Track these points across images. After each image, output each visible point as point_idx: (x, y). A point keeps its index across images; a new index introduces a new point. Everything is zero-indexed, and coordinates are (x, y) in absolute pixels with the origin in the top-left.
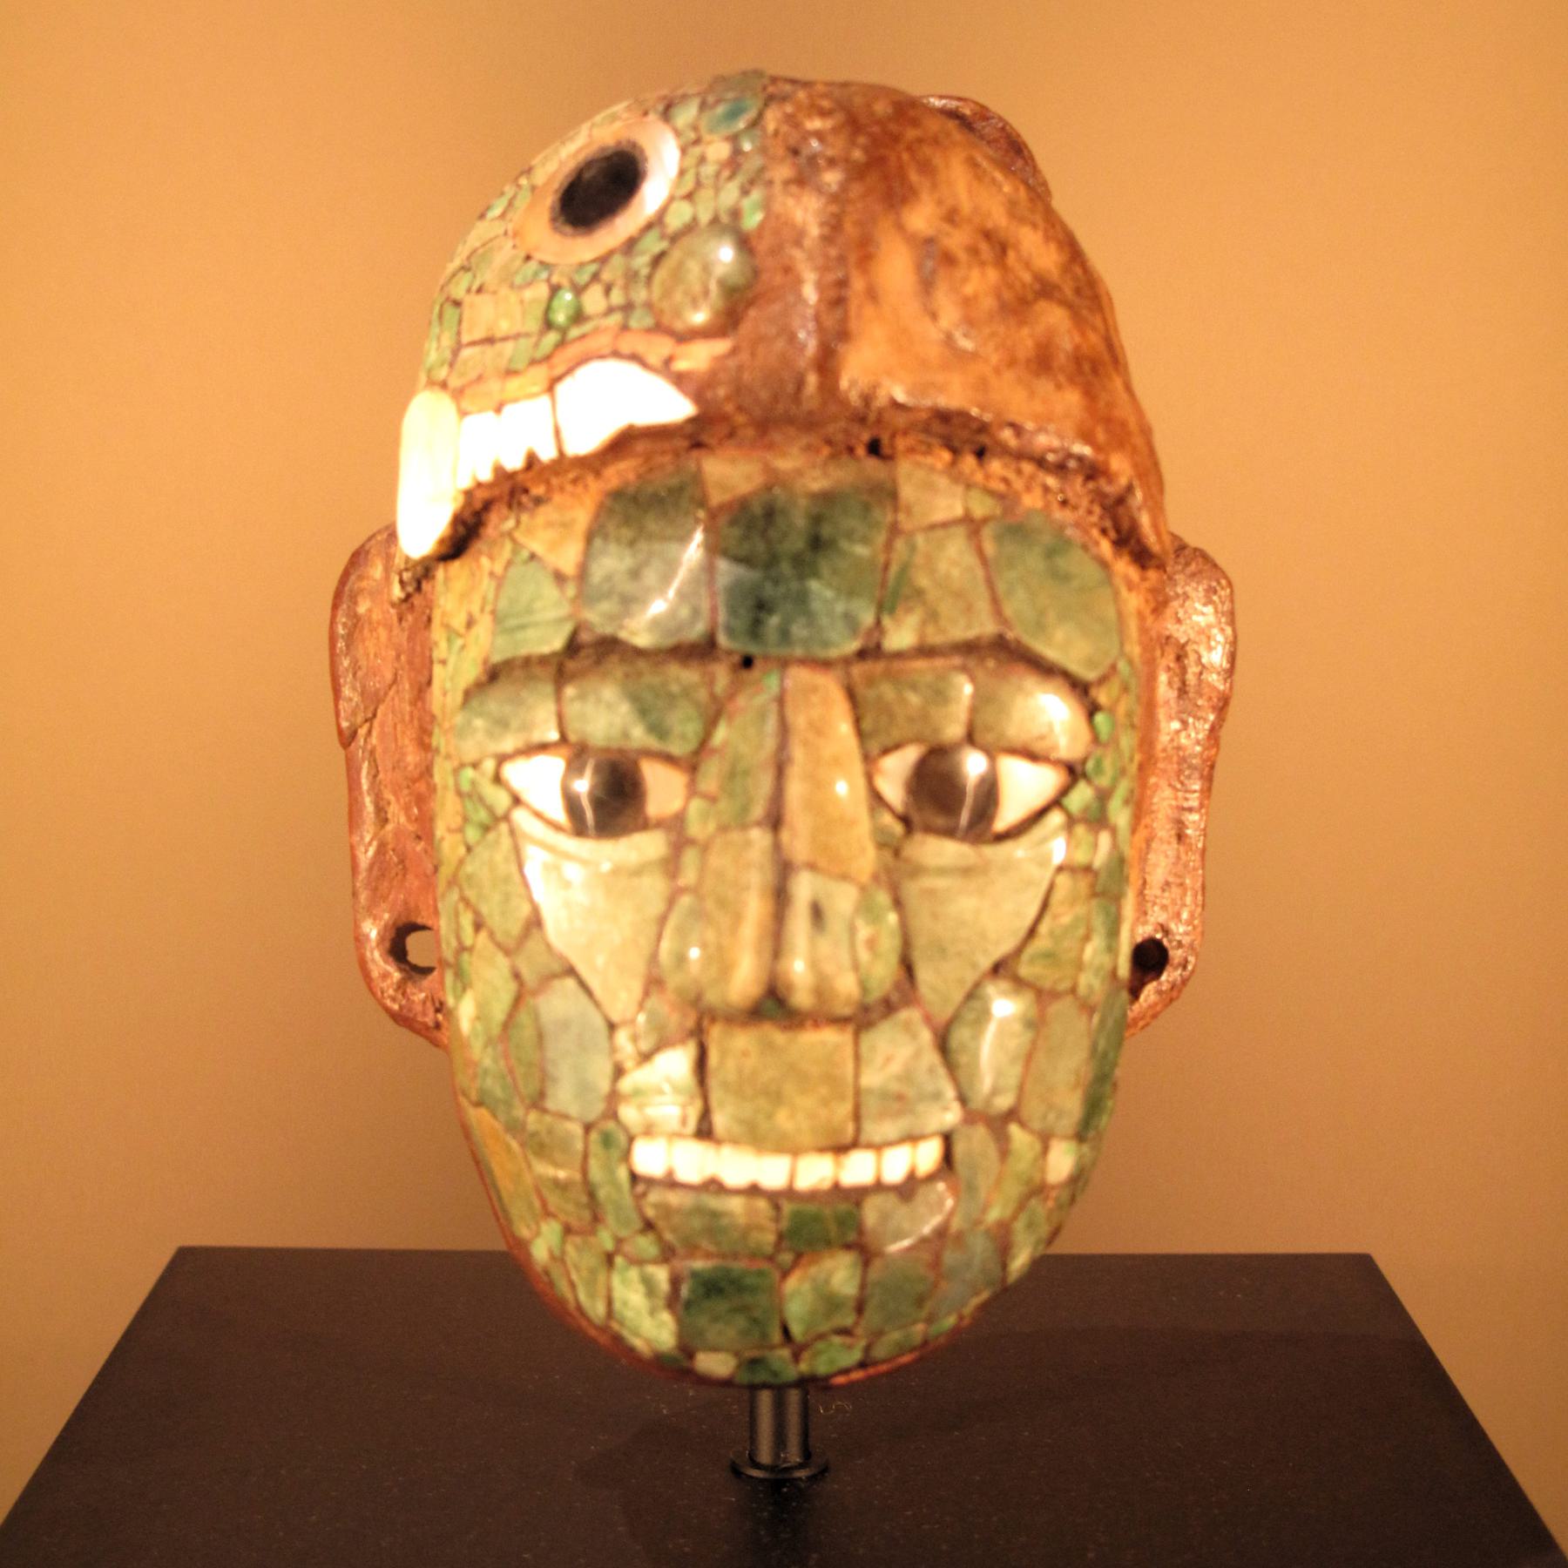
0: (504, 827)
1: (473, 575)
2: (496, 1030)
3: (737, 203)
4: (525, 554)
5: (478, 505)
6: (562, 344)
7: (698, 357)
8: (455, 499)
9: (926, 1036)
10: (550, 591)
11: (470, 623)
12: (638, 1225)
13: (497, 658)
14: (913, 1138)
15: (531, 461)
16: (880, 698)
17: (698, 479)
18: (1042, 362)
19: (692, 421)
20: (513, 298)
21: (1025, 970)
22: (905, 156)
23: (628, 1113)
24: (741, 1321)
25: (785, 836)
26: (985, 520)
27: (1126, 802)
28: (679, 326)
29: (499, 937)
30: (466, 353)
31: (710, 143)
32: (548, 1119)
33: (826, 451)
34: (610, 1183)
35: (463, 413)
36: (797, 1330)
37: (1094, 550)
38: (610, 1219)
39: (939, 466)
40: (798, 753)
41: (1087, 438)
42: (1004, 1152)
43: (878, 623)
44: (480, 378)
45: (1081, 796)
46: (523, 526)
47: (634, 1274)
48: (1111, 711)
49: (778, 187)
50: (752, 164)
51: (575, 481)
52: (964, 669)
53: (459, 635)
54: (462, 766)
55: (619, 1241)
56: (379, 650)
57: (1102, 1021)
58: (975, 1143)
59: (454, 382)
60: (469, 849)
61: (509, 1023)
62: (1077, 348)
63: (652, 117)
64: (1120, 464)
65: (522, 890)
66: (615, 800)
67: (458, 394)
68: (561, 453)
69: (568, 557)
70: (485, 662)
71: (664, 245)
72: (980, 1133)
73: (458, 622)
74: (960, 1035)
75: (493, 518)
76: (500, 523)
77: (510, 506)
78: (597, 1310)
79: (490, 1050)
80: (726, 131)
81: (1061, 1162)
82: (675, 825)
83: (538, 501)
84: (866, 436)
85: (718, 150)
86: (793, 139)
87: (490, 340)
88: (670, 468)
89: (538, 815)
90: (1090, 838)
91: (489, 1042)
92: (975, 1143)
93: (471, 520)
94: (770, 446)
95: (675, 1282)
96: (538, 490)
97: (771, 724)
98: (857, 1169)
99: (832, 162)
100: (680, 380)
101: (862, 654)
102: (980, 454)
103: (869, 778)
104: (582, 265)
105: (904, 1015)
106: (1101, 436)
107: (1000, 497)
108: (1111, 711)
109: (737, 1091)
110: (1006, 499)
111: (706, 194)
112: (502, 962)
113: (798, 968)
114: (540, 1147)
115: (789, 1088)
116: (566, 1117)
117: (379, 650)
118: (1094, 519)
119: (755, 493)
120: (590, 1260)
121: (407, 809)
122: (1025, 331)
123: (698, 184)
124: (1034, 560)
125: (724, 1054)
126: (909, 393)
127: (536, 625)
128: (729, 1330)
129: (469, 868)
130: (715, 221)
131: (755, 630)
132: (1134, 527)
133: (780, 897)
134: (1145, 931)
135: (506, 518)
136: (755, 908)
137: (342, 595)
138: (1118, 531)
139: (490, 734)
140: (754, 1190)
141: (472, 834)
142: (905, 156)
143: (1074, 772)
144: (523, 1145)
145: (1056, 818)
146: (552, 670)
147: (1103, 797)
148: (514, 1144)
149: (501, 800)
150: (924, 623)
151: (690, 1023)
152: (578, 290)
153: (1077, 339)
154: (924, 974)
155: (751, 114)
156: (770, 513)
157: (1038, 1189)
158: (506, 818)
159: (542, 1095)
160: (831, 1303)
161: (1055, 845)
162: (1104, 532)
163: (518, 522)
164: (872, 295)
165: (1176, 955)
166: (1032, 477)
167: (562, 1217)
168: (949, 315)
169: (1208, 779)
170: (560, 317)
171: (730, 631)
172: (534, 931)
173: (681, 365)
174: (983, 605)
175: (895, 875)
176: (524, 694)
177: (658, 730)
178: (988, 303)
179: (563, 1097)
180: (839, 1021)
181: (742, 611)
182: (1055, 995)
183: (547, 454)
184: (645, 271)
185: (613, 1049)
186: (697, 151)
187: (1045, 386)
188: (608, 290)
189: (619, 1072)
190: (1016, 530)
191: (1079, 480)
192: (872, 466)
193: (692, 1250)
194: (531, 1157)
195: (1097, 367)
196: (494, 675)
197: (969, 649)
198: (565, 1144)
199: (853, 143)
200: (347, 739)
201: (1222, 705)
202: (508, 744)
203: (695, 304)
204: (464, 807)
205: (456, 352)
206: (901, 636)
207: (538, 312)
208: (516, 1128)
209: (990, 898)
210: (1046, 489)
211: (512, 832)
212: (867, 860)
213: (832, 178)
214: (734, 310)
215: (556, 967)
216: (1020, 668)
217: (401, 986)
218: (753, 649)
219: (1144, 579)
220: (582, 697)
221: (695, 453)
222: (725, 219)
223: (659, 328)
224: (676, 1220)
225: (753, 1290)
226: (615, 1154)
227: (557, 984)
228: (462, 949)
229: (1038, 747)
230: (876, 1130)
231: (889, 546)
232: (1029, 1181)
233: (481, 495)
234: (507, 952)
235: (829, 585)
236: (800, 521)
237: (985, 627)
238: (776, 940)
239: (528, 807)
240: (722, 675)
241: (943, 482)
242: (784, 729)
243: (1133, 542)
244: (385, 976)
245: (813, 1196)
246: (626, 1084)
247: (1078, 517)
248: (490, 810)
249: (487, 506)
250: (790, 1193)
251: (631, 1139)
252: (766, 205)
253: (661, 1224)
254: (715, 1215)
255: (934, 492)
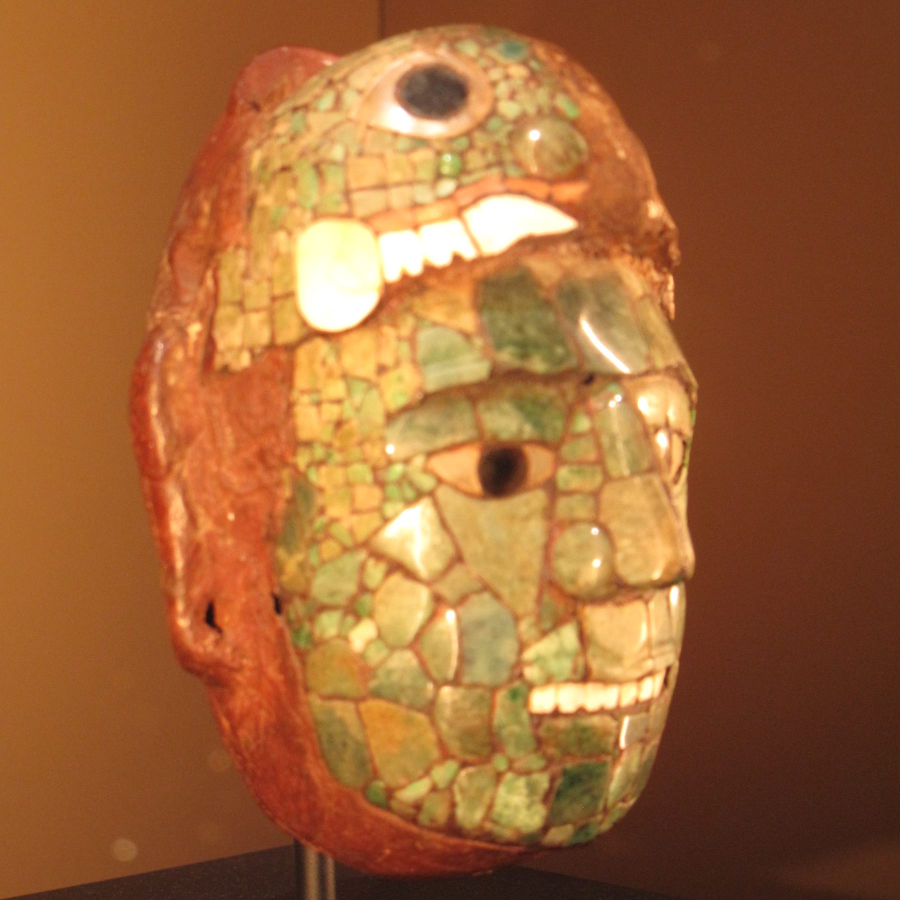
35: (377, 233)
183: (469, 254)
189: (522, 647)
220: (489, 409)
226: (520, 701)
254: (585, 730)
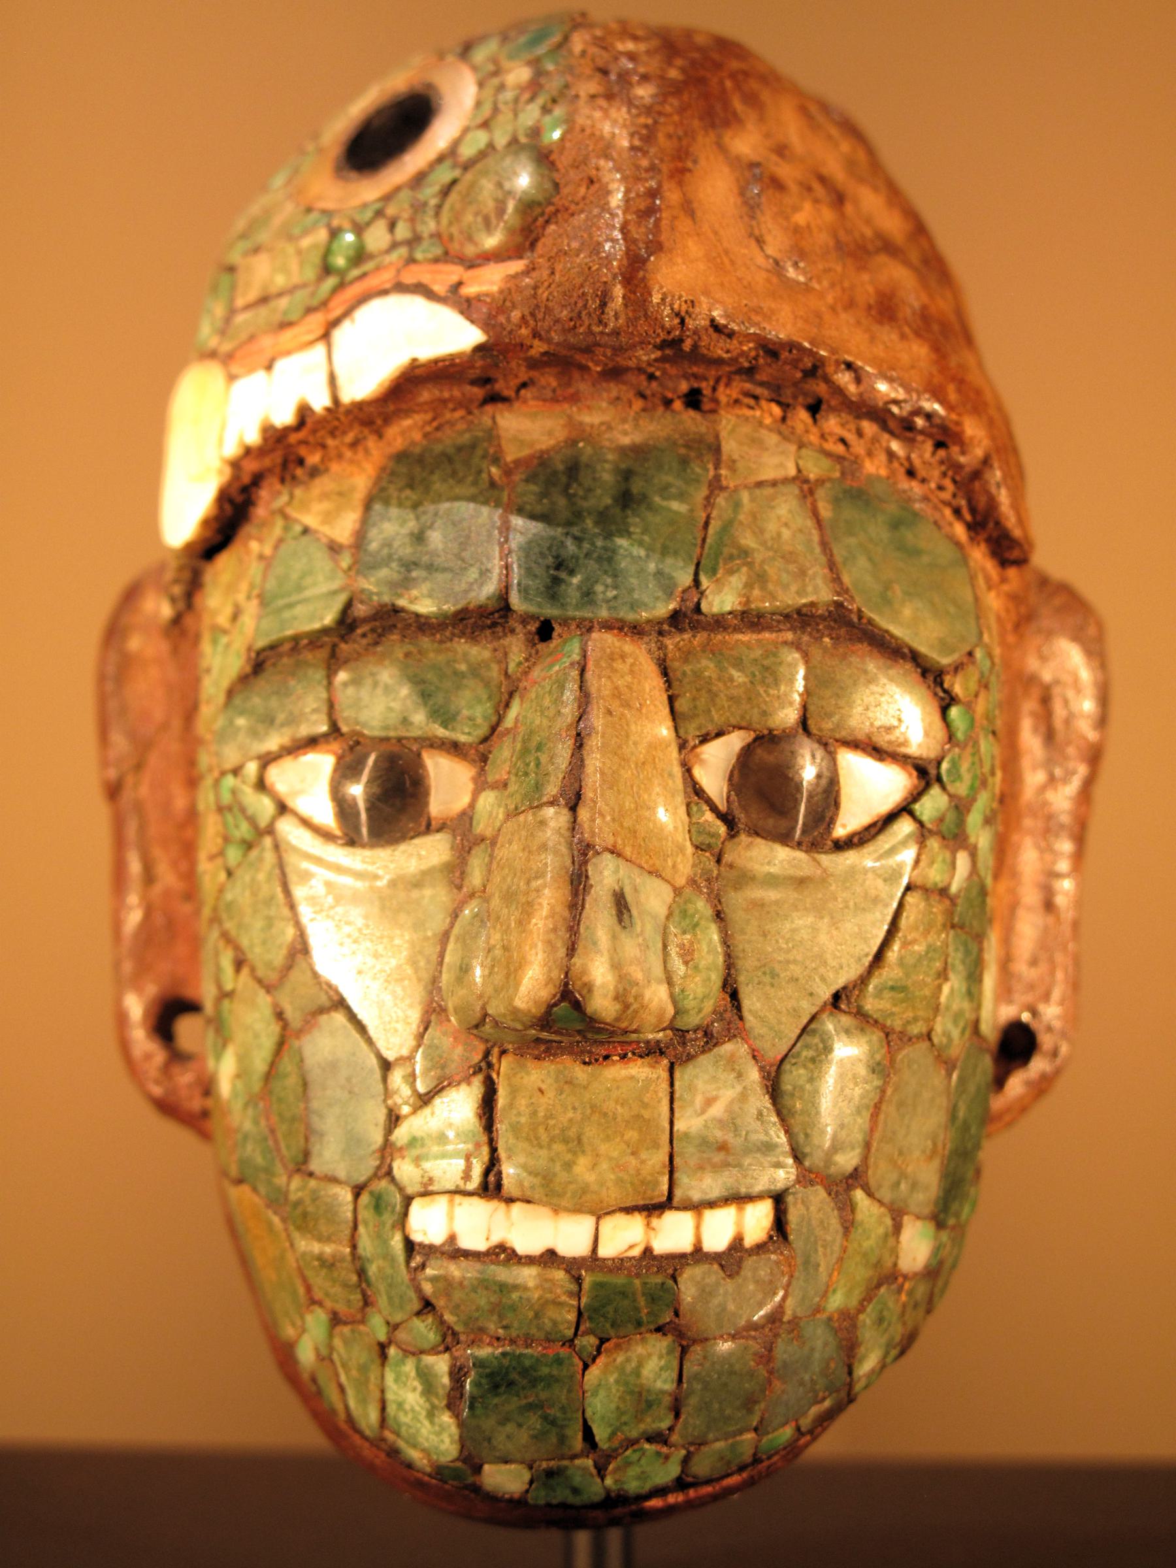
0: (268, 841)
1: (240, 561)
2: (257, 1086)
3: (538, 121)
4: (298, 529)
5: (246, 479)
6: (341, 286)
7: (488, 281)
8: (220, 472)
9: (754, 1075)
10: (321, 561)
11: (235, 616)
12: (416, 1305)
13: (261, 643)
14: (739, 1199)
15: (304, 412)
16: (698, 675)
17: (492, 435)
18: (885, 309)
19: (479, 349)
20: (290, 249)
21: (871, 1004)
22: (729, 84)
23: (404, 1170)
24: (534, 1421)
25: (583, 814)
26: (821, 482)
27: (988, 821)
28: (470, 251)
29: (260, 973)
30: (240, 319)
31: (509, 71)
32: (313, 1183)
33: (638, 404)
34: (380, 1250)
36: (601, 1433)
37: (947, 529)
38: (383, 1301)
39: (768, 421)
40: (597, 719)
41: (938, 394)
42: (848, 1226)
43: (697, 582)
44: (252, 338)
45: (932, 805)
46: (296, 502)
47: (409, 1367)
48: (969, 707)
49: (582, 102)
50: (553, 85)
51: (354, 445)
52: (797, 646)
53: (225, 632)
54: (223, 773)
55: (393, 1327)
56: (148, 690)
57: (962, 1080)
58: (812, 1209)
59: (226, 347)
60: (230, 874)
61: (270, 1074)
62: (924, 308)
63: (450, 58)
64: (972, 429)
65: (286, 912)
66: (393, 800)
67: (227, 359)
68: (336, 400)
69: (344, 528)
70: (249, 649)
71: (457, 173)
72: (818, 1195)
73: (223, 620)
74: (794, 1076)
75: (263, 493)
76: (269, 500)
77: (282, 481)
78: (369, 1418)
79: (250, 1112)
80: (528, 56)
81: (916, 1246)
82: (461, 827)
83: (314, 473)
84: (684, 387)
85: (519, 74)
86: (603, 57)
87: (264, 300)
88: (461, 426)
89: (306, 823)
90: (948, 855)
91: (251, 1101)
92: (812, 1209)
93: (239, 499)
94: (574, 399)
95: (457, 1374)
96: (313, 459)
97: (570, 694)
98: (674, 1233)
99: (645, 78)
100: (467, 308)
101: (675, 618)
102: (814, 409)
103: (688, 771)
104: (365, 206)
105: (727, 1048)
106: (953, 396)
107: (839, 459)
108: (969, 707)
109: (531, 1136)
110: (847, 464)
111: (506, 116)
112: (264, 1000)
113: (599, 973)
114: (304, 1219)
115: (591, 1132)
116: (334, 1180)
117: (148, 690)
118: (946, 495)
119: (556, 449)
120: (361, 1355)
121: (174, 864)
122: (865, 277)
123: (496, 110)
124: (878, 530)
125: (514, 1092)
126: (727, 316)
127: (306, 600)
128: (516, 1435)
129: (229, 896)
130: (514, 141)
131: (553, 589)
132: (993, 504)
133: (578, 884)
134: (1007, 1013)
135: (279, 493)
136: (549, 899)
137: (114, 632)
138: (973, 510)
139: (254, 734)
140: (550, 1257)
141: (233, 855)
142: (729, 84)
143: (925, 774)
144: (284, 1220)
145: (905, 827)
146: (323, 653)
147: (961, 807)
148: (276, 1220)
149: (264, 806)
150: (749, 586)
151: (477, 1057)
152: (359, 229)
153: (925, 298)
154: (751, 1002)
155: (556, 38)
156: (574, 469)
157: (890, 1277)
158: (270, 830)
159: (306, 1155)
160: (643, 1401)
161: (900, 853)
162: (957, 512)
163: (292, 496)
164: (688, 208)
165: (1046, 1041)
166: (875, 440)
167: (329, 1304)
168: (776, 243)
169: (1080, 839)
170: (340, 261)
171: (524, 591)
172: (299, 957)
173: (470, 290)
174: (818, 571)
175: (716, 884)
176: (292, 683)
177: (444, 716)
178: (823, 238)
179: (329, 1156)
180: (653, 1051)
181: (538, 571)
182: (906, 1038)
184: (433, 202)
185: (387, 1093)
186: (495, 81)
187: (887, 335)
188: (392, 226)
189: (394, 1119)
190: (857, 495)
191: (929, 446)
192: (690, 420)
193: (478, 1335)
194: (296, 1235)
195: (947, 333)
196: (259, 664)
197: (802, 619)
198: (331, 1212)
199: (669, 63)
200: (113, 791)
201: (1094, 756)
202: (273, 743)
203: (488, 226)
204: (225, 824)
205: (228, 320)
206: (722, 599)
207: (316, 258)
208: (278, 1200)
209: (831, 919)
210: (891, 455)
211: (277, 847)
212: (685, 865)
213: (644, 92)
214: (532, 226)
215: (323, 1000)
216: (864, 647)
217: (166, 1068)
218: (550, 611)
219: (1004, 580)
220: (356, 682)
221: (489, 408)
222: (523, 140)
223: (447, 257)
224: (458, 1295)
225: (550, 1381)
226: (389, 1219)
227: (324, 1019)
228: (225, 995)
229: (882, 740)
230: (693, 1186)
231: (709, 502)
232: (878, 1264)
233: (251, 466)
234: (269, 989)
235: (641, 544)
236: (607, 476)
237: (820, 593)
238: (572, 935)
239: (295, 814)
240: (516, 648)
241: (772, 439)
242: (584, 698)
243: (991, 525)
244: (148, 1057)
245: (619, 1264)
246: (401, 1134)
247: (928, 494)
248: (252, 821)
249: (257, 480)
250: (593, 1260)
251: (408, 1200)
252: (569, 122)
253: (440, 1303)
254: (504, 1288)
255: (762, 449)
